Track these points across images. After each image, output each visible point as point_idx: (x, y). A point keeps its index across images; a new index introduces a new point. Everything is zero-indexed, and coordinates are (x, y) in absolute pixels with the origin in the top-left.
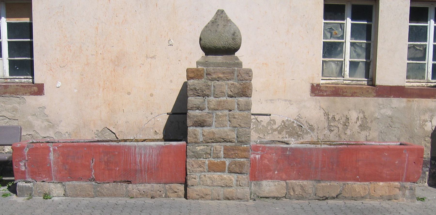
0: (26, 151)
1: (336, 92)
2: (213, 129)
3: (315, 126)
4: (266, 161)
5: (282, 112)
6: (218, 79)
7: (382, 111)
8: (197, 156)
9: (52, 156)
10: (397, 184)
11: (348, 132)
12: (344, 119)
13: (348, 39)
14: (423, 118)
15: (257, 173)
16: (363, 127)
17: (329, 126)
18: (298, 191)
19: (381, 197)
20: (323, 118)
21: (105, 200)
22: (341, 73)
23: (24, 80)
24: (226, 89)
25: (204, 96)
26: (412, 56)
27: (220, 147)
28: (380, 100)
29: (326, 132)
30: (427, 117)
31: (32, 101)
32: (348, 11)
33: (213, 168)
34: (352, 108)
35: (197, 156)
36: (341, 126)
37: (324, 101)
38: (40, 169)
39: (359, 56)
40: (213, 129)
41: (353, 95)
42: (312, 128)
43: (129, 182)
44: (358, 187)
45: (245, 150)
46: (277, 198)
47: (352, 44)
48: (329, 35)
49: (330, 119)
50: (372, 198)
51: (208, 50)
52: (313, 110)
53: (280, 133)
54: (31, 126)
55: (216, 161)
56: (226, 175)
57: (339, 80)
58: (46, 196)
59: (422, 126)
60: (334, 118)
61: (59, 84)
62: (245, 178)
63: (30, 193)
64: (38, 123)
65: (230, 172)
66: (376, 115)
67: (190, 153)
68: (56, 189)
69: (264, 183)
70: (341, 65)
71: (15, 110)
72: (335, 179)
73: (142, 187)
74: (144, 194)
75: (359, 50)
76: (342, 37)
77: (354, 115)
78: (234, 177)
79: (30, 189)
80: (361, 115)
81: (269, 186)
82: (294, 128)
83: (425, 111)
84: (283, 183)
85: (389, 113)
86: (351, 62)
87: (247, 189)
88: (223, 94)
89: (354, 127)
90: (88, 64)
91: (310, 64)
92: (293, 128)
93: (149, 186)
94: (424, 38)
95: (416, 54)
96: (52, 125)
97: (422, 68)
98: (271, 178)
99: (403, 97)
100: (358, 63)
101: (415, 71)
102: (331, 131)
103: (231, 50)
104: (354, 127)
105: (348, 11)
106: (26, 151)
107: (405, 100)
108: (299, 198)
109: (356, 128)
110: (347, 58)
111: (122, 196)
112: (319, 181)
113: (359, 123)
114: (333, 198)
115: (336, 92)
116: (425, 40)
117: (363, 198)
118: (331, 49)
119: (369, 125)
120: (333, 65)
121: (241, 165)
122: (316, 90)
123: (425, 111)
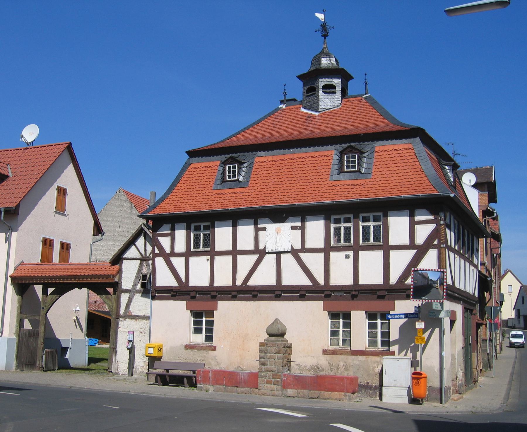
0: (201, 372)
1: (334, 353)
2: (268, 366)
3: (325, 369)
4: (289, 381)
5: (310, 362)
6: (271, 346)
7: (355, 362)
8: (262, 377)
9: (210, 375)
10: (343, 393)
11: (339, 372)
12: (337, 365)
13: (341, 329)
14: (374, 366)
15: (285, 386)
16: (346, 369)
17: (331, 369)
18: (302, 394)
19: (336, 399)
20: (328, 365)
21: (229, 393)
22: (338, 344)
23: (209, 344)
24: (273, 351)
25: (265, 353)
26: (370, 336)
27: (270, 374)
28: (353, 357)
29: (330, 371)
30: (375, 365)
31: (212, 353)
32: (341, 316)
33: (269, 382)
34: (341, 360)
35: (262, 377)
36: (336, 369)
37: (328, 357)
38: (206, 380)
39: (346, 336)
40: (268, 366)
41: (341, 354)
42: (323, 370)
43: (237, 387)
44: (326, 394)
45: (280, 376)
46: (293, 397)
47: (343, 331)
48: (333, 327)
49: (331, 365)
50: (332, 399)
51: (270, 335)
52: (323, 361)
53: (309, 371)
54: (210, 364)
55: (269, 379)
56: (272, 386)
57: (337, 347)
58: (207, 391)
59: (373, 370)
60: (332, 365)
61: (222, 346)
62: (279, 387)
63: (201, 389)
64: (213, 363)
65: (274, 384)
66: (352, 364)
67: (259, 376)
68: (211, 388)
69: (289, 390)
70: (338, 340)
71: (205, 357)
72: (317, 390)
73: (242, 389)
74: (242, 392)
75: (347, 334)
76: (339, 328)
77: (341, 364)
78: (275, 387)
79: (202, 387)
80: (345, 364)
81: (290, 392)
82: (315, 368)
83: (374, 363)
84: (296, 391)
85: (358, 363)
86: (343, 339)
87: (280, 392)
88: (272, 352)
89: (342, 369)
90: (233, 338)
91: (326, 341)
92: (315, 369)
93: (245, 389)
94: (376, 328)
95: (372, 335)
96: (218, 364)
97: (376, 342)
98: (291, 388)
99: (364, 355)
100: (346, 340)
101: (373, 343)
102: (332, 371)
103: (282, 335)
104: (342, 369)
105: (341, 316)
106: (201, 372)
107: (365, 357)
108: (302, 397)
109: (343, 370)
110: (341, 337)
111: (235, 392)
112: (310, 390)
113: (344, 367)
114: (316, 398)
115: (334, 353)
116: (377, 328)
117: (328, 399)
118: (334, 333)
119: (349, 368)
120: (335, 341)
121: (278, 382)
122: (325, 352)
123: (374, 363)
